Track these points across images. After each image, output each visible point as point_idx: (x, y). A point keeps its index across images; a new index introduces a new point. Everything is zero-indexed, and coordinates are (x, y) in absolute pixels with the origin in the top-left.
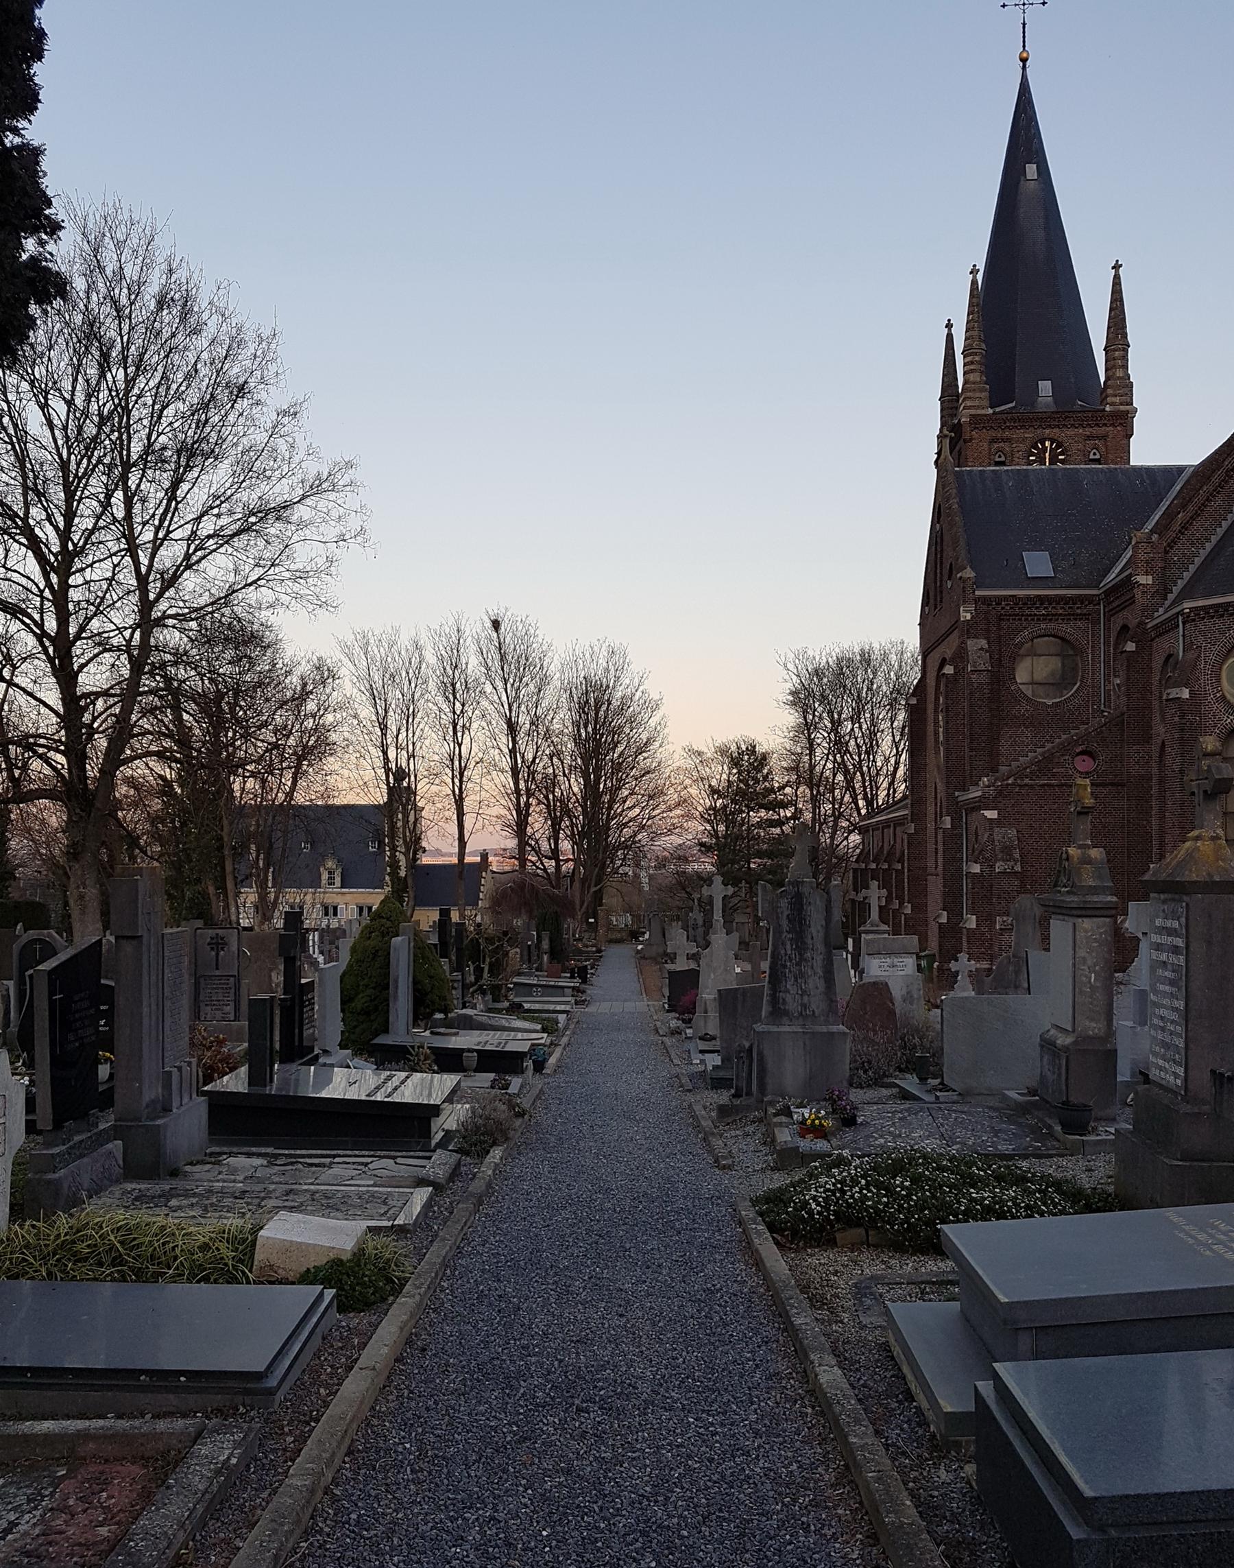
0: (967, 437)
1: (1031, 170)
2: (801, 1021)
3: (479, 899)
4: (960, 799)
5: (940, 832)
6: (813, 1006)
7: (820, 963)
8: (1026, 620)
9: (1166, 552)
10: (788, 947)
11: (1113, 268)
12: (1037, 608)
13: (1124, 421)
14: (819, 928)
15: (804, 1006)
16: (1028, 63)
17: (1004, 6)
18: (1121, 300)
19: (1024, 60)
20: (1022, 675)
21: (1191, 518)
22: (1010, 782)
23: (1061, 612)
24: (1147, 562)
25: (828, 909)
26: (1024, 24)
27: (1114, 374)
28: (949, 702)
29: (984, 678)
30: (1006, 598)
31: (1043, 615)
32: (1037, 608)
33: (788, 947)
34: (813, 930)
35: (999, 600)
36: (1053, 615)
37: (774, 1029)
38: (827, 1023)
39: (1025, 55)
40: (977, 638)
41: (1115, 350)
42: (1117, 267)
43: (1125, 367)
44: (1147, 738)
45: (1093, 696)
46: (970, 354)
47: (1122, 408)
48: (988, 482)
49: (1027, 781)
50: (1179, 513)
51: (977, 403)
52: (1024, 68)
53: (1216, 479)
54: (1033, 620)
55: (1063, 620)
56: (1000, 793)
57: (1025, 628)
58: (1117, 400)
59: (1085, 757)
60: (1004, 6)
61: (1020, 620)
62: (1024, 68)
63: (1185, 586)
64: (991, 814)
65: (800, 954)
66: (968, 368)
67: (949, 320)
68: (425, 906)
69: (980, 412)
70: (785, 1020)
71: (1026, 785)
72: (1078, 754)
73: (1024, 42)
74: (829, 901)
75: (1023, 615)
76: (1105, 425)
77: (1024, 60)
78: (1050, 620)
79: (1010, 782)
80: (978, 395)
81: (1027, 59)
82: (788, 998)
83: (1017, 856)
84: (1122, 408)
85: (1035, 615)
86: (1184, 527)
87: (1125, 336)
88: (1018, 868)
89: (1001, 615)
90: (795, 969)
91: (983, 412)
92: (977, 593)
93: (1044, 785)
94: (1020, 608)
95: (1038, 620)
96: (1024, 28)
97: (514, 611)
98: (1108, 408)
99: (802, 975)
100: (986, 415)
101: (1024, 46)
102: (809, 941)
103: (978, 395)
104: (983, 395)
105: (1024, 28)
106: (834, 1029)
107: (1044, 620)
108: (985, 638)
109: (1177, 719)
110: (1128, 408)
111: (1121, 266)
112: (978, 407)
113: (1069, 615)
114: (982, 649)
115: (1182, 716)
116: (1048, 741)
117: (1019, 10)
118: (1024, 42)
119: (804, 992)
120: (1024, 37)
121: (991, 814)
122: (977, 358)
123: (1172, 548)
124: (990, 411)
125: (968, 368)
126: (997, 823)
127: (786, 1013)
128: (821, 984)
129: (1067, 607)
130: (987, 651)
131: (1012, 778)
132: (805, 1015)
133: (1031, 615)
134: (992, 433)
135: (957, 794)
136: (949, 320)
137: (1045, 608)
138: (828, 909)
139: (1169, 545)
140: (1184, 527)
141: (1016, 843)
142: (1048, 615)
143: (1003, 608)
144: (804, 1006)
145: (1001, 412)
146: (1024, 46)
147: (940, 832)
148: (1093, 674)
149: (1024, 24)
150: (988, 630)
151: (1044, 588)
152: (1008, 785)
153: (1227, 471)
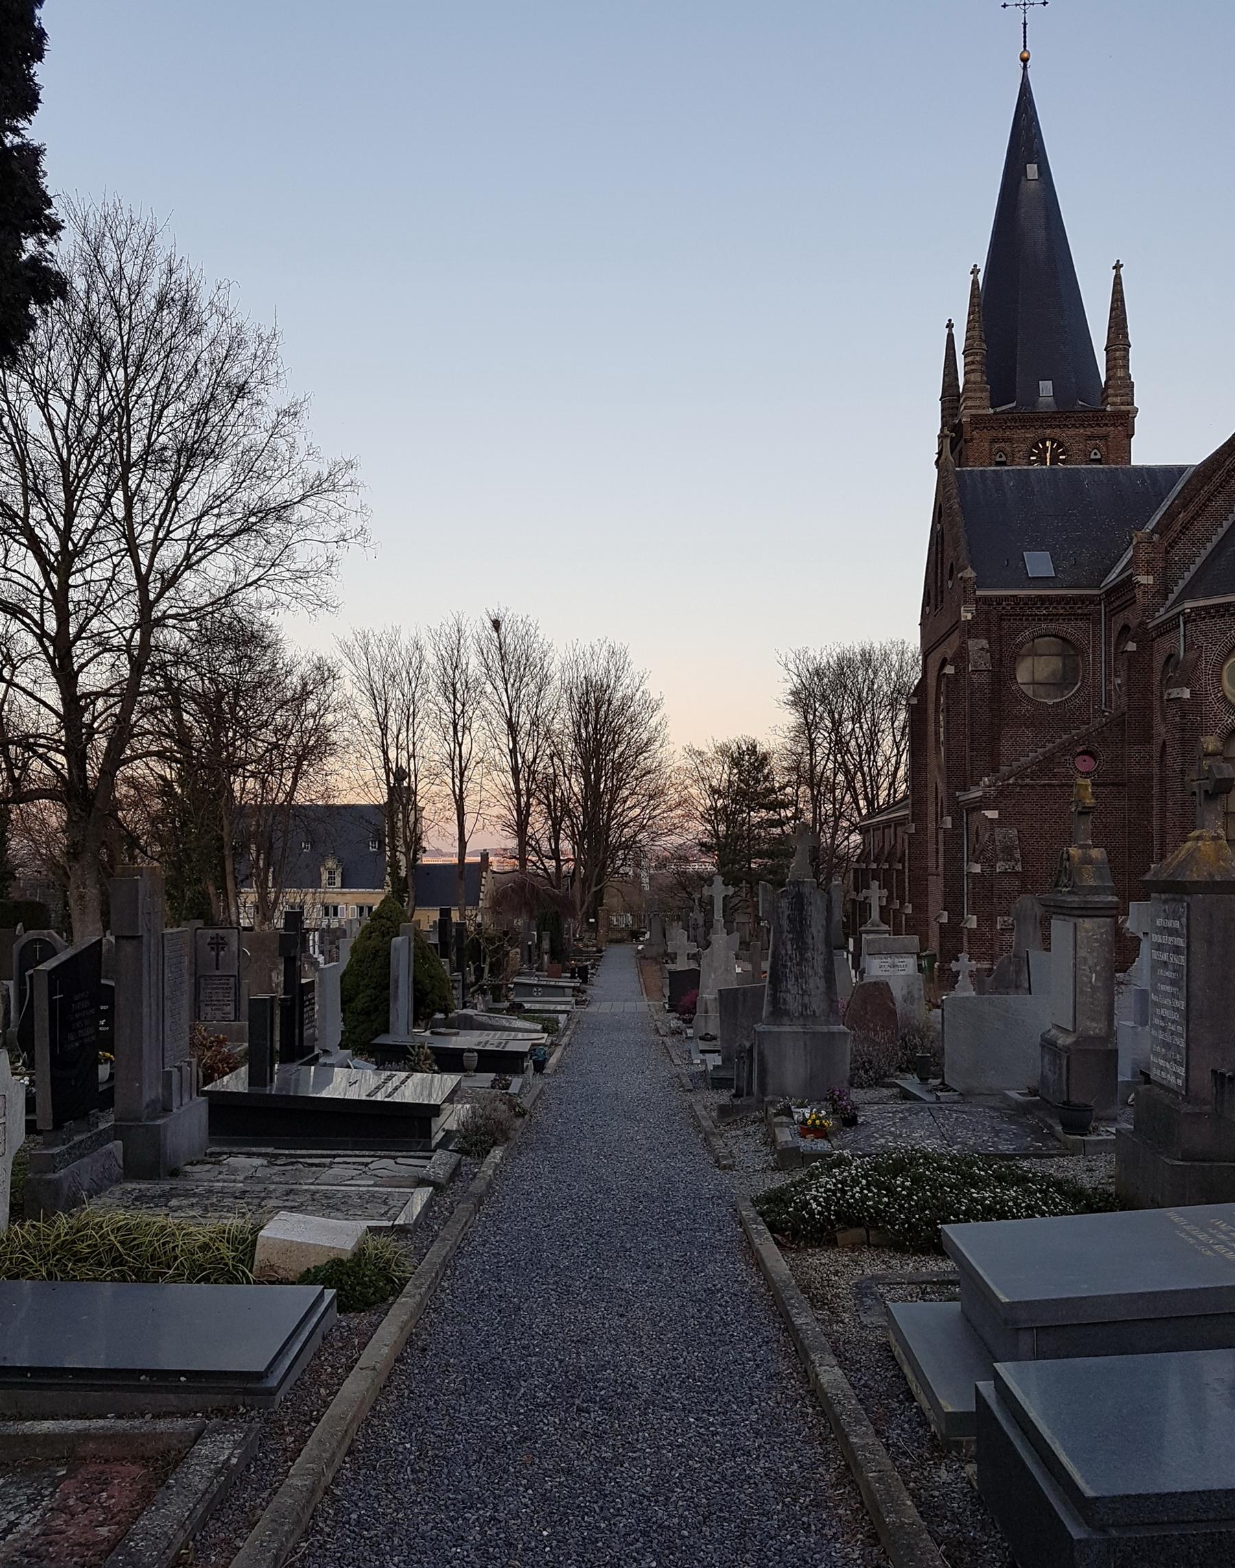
0: (968, 437)
1: (1032, 170)
2: (801, 1021)
3: (479, 899)
4: (961, 799)
5: (941, 832)
6: (814, 1006)
7: (820, 963)
8: (1027, 620)
9: (1167, 552)
10: (789, 947)
11: (1114, 268)
12: (1038, 608)
13: (1124, 421)
14: (820, 928)
15: (805, 1006)
16: (1029, 63)
17: (1005, 6)
18: (1122, 300)
19: (1025, 60)
20: (1022, 675)
21: (1192, 518)
22: (1011, 782)
23: (1062, 612)
24: (1148, 562)
25: (829, 909)
26: (1025, 24)
27: (1115, 374)
28: (950, 702)
29: (985, 678)
30: (1006, 598)
31: (1044, 615)
32: (1038, 608)
33: (789, 947)
34: (813, 930)
35: (1000, 600)
36: (1054, 615)
37: (775, 1029)
38: (827, 1023)
39: (1026, 55)
40: (978, 638)
41: (1116, 350)
42: (1118, 267)
43: (1126, 367)
44: (1148, 738)
45: (1094, 696)
46: (971, 354)
47: (1123, 408)
48: (988, 482)
49: (1028, 781)
50: (1180, 513)
51: (977, 403)
52: (1025, 68)
53: (1217, 479)
54: (1034, 620)
55: (1064, 620)
56: (1001, 793)
57: (1026, 628)
58: (1118, 400)
59: (1086, 757)
60: (1005, 6)
61: (1021, 620)
62: (1025, 68)
63: (1186, 586)
64: (992, 814)
65: (801, 954)
66: (969, 368)
67: (950, 320)
68: (425, 906)
69: (980, 412)
70: (786, 1020)
71: (1027, 785)
72: (1079, 754)
73: (1025, 42)
74: (830, 901)
75: (1023, 615)
76: (1106, 425)
77: (1025, 60)
78: (1051, 620)
79: (1011, 782)
80: (978, 395)
81: (1028, 59)
82: (789, 998)
83: (1018, 856)
84: (1123, 408)
85: (1036, 615)
86: (1185, 527)
87: (1126, 336)
88: (1019, 868)
89: (1002, 615)
90: (796, 969)
91: (984, 412)
92: (977, 593)
93: (1044, 785)
94: (1021, 608)
95: (1039, 620)
96: (1025, 28)
97: (514, 611)
98: (1109, 408)
99: (802, 975)
100: (987, 415)
101: (1025, 46)
102: (810, 941)
103: (978, 395)
104: (984, 395)
105: (1025, 28)
106: (834, 1029)
107: (1045, 620)
108: (986, 638)
109: (1178, 719)
110: (1129, 408)
111: (1122, 266)
112: (979, 407)
113: (1070, 615)
114: (982, 649)
115: (1183, 716)
116: (1049, 741)
117: (1020, 10)
118: (1025, 42)
119: (805, 992)
120: (1025, 37)
121: (992, 814)
122: (978, 358)
123: (1172, 548)
124: (991, 411)
125: (969, 368)
126: (998, 823)
127: (787, 1013)
128: (822, 984)
129: (1067, 607)
130: (988, 651)
131: (1013, 778)
132: (806, 1015)
133: (1031, 615)
134: (993, 433)
135: (957, 794)
136: (950, 320)
137: (1046, 608)
138: (829, 909)
139: (1170, 545)
140: (1185, 527)
141: (1017, 843)
142: (1049, 615)
143: (1004, 608)
144: (805, 1006)
145: (1002, 412)
146: (1025, 46)
147: (941, 832)
148: (1094, 674)
149: (1025, 24)
150: (988, 630)
151: (1045, 588)
152: (1009, 785)
153: (1228, 471)
